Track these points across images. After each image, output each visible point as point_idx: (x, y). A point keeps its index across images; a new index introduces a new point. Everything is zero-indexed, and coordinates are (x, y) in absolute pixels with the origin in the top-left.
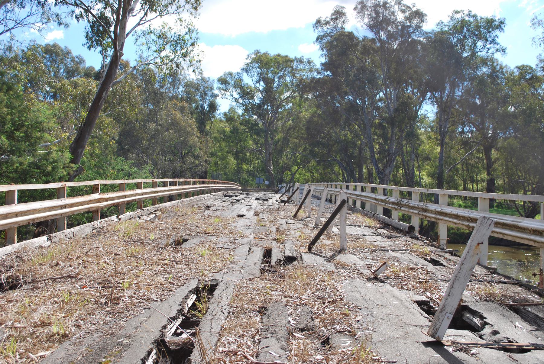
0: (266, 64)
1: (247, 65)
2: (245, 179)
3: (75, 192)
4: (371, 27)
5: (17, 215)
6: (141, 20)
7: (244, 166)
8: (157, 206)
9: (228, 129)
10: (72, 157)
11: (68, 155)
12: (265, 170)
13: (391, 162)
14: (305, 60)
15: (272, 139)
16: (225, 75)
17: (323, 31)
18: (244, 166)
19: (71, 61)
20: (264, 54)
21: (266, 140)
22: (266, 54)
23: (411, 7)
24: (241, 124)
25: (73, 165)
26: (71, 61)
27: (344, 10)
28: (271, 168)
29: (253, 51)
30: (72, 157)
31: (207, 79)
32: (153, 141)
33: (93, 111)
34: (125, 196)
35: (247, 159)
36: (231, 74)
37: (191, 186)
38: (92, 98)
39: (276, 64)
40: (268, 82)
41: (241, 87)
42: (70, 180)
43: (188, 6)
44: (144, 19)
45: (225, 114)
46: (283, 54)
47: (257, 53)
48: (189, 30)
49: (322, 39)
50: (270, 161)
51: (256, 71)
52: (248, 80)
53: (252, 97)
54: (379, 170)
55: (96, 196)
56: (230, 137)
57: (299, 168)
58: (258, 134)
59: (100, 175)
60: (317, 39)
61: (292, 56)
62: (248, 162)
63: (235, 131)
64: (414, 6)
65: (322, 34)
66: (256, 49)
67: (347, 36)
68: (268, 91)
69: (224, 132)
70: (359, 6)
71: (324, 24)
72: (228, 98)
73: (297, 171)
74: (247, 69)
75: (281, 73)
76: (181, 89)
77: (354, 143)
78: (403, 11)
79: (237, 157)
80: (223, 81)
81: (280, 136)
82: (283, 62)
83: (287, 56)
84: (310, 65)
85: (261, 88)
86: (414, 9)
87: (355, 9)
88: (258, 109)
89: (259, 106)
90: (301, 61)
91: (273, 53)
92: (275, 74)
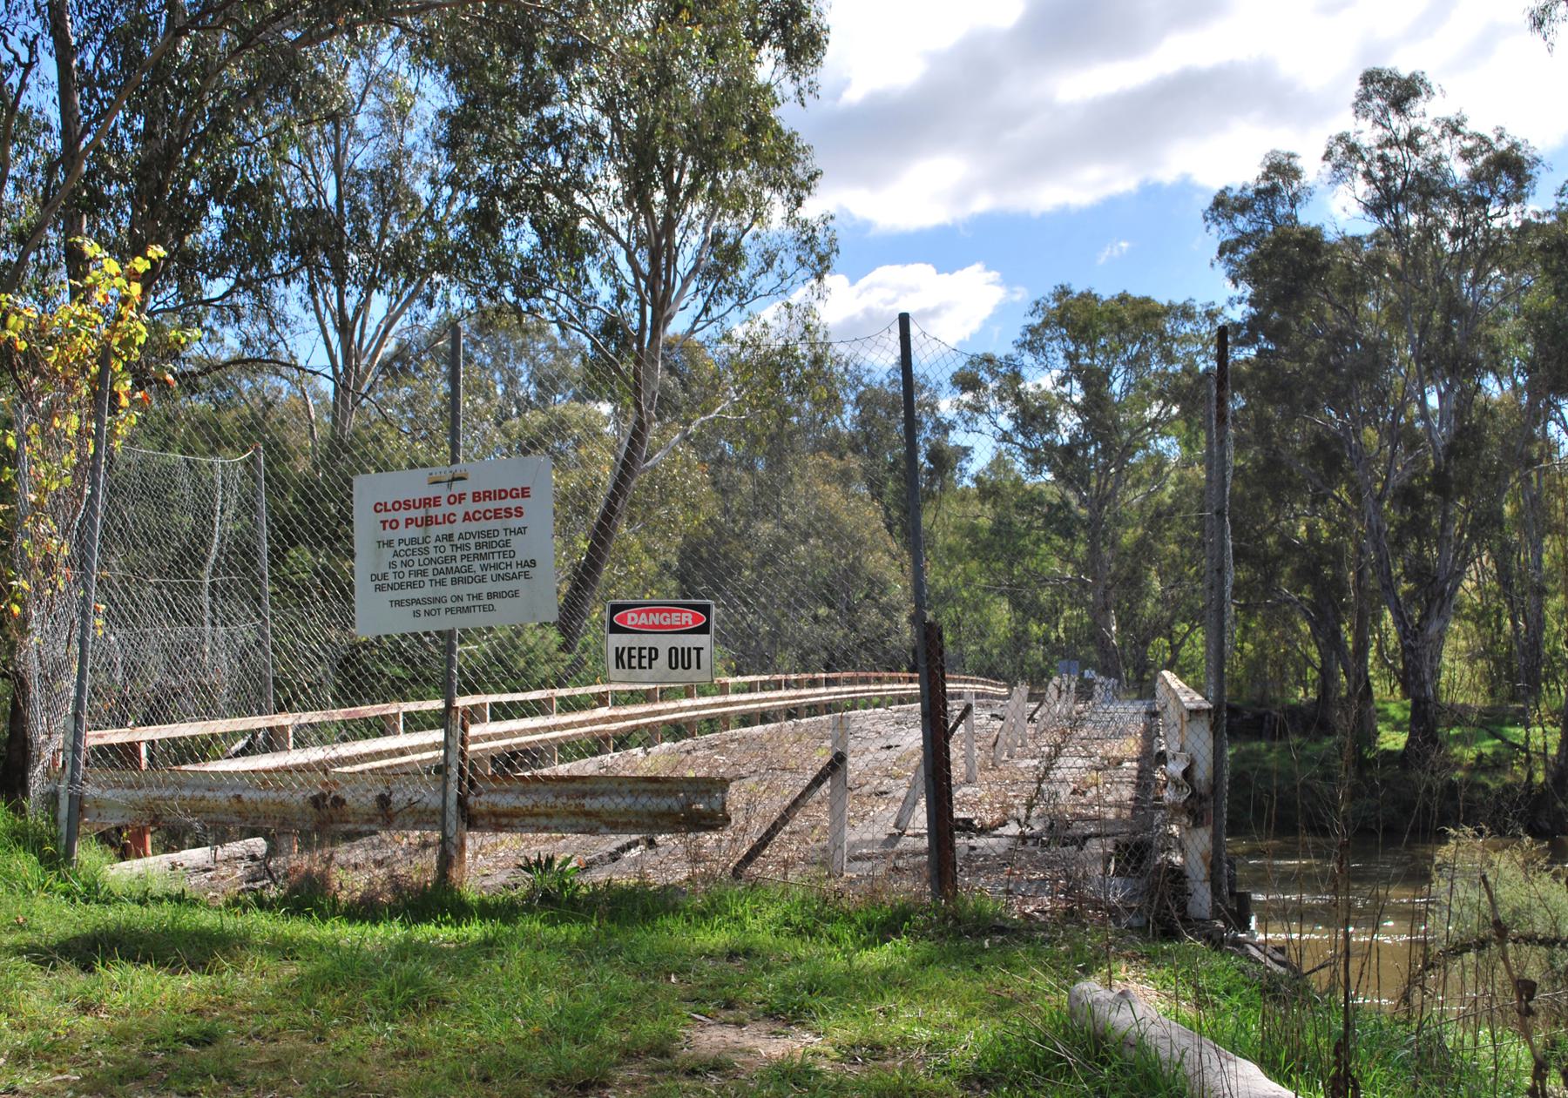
0: (1084, 330)
1: (1032, 330)
2: (1037, 664)
3: (568, 705)
4: (1375, 209)
5: (489, 738)
6: (697, 319)
7: (1035, 629)
8: (732, 731)
9: (985, 522)
10: (560, 640)
11: (554, 637)
12: (1095, 636)
13: (1443, 602)
14: (1198, 309)
15: (1113, 545)
16: (971, 362)
17: (1235, 230)
18: (1035, 629)
19: (549, 348)
20: (1082, 295)
21: (1093, 550)
22: (1088, 298)
23: (1493, 137)
24: (1020, 507)
25: (562, 655)
26: (549, 348)
27: (1298, 163)
28: (1110, 631)
29: (1052, 290)
30: (560, 640)
31: (922, 381)
32: (770, 570)
33: (602, 534)
34: (659, 713)
35: (1040, 608)
36: (988, 360)
37: (822, 690)
38: (602, 496)
39: (1115, 326)
40: (1094, 381)
41: (1019, 398)
42: (561, 685)
43: (803, 273)
44: (703, 317)
45: (977, 479)
46: (1136, 292)
47: (1064, 292)
48: (807, 328)
49: (1234, 250)
50: (1106, 608)
51: (1057, 352)
52: (1041, 379)
53: (1051, 425)
54: (1406, 626)
55: (603, 712)
56: (988, 546)
57: (1192, 628)
58: (1068, 534)
59: (764, 669)
60: (1221, 252)
61: (1162, 298)
62: (1048, 615)
63: (1002, 528)
64: (1500, 137)
65: (1232, 237)
66: (1058, 283)
67: (1300, 243)
68: (1096, 406)
69: (973, 531)
70: (1340, 150)
71: (1235, 209)
72: (984, 429)
73: (1186, 635)
74: (1033, 341)
75: (1133, 349)
76: (849, 413)
77: (1337, 551)
78: (1467, 155)
79: (1016, 604)
80: (966, 381)
81: (1128, 537)
82: (1136, 320)
83: (1147, 300)
84: (1213, 322)
85: (1077, 399)
86: (1503, 146)
87: (1328, 156)
88: (1066, 460)
89: (1069, 451)
90: (1186, 313)
91: (1107, 291)
92: (1111, 353)
